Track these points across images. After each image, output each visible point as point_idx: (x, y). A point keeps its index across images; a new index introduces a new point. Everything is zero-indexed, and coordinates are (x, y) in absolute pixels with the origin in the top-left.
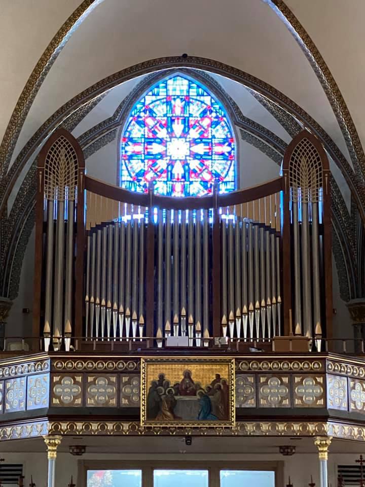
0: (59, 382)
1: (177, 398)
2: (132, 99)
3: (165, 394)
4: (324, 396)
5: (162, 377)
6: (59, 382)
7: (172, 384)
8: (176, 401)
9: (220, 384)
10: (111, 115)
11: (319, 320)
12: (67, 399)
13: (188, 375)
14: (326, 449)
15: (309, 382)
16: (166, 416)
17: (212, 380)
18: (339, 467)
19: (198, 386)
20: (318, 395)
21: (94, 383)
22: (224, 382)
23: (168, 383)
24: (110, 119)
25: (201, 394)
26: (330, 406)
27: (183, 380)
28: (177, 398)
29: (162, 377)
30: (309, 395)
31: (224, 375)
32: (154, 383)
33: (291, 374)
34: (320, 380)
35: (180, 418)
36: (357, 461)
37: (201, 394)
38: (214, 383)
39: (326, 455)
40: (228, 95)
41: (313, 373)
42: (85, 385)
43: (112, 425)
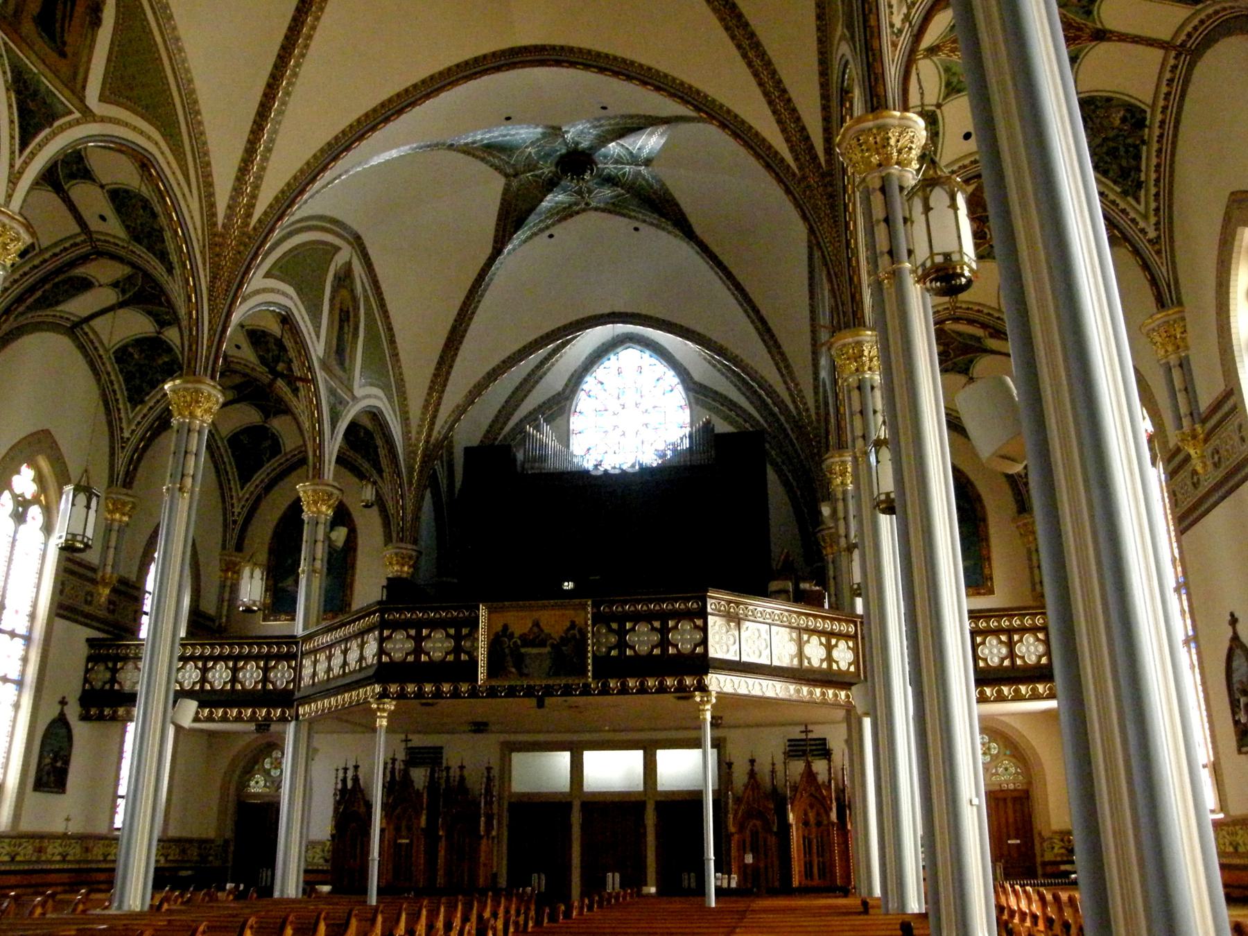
0: (389, 637)
1: (523, 650)
2: (979, 323)
3: (509, 646)
4: (704, 642)
5: (505, 627)
6: (389, 637)
7: (517, 635)
8: (523, 655)
9: (576, 632)
10: (560, 389)
11: (189, 580)
12: (398, 656)
13: (536, 624)
14: (385, 714)
15: (686, 626)
16: (511, 672)
17: (565, 628)
18: (789, 740)
19: (549, 636)
20: (697, 642)
21: (429, 636)
22: (580, 630)
23: (512, 635)
24: (559, 394)
25: (552, 646)
26: (712, 653)
27: (531, 629)
28: (523, 650)
29: (505, 627)
30: (396, 651)
31: (579, 621)
32: (497, 634)
33: (419, 625)
34: (699, 622)
35: (527, 675)
36: (802, 732)
37: (552, 646)
38: (569, 630)
39: (385, 723)
40: (726, 349)
41: (688, 615)
42: (418, 639)
43: (614, 681)
